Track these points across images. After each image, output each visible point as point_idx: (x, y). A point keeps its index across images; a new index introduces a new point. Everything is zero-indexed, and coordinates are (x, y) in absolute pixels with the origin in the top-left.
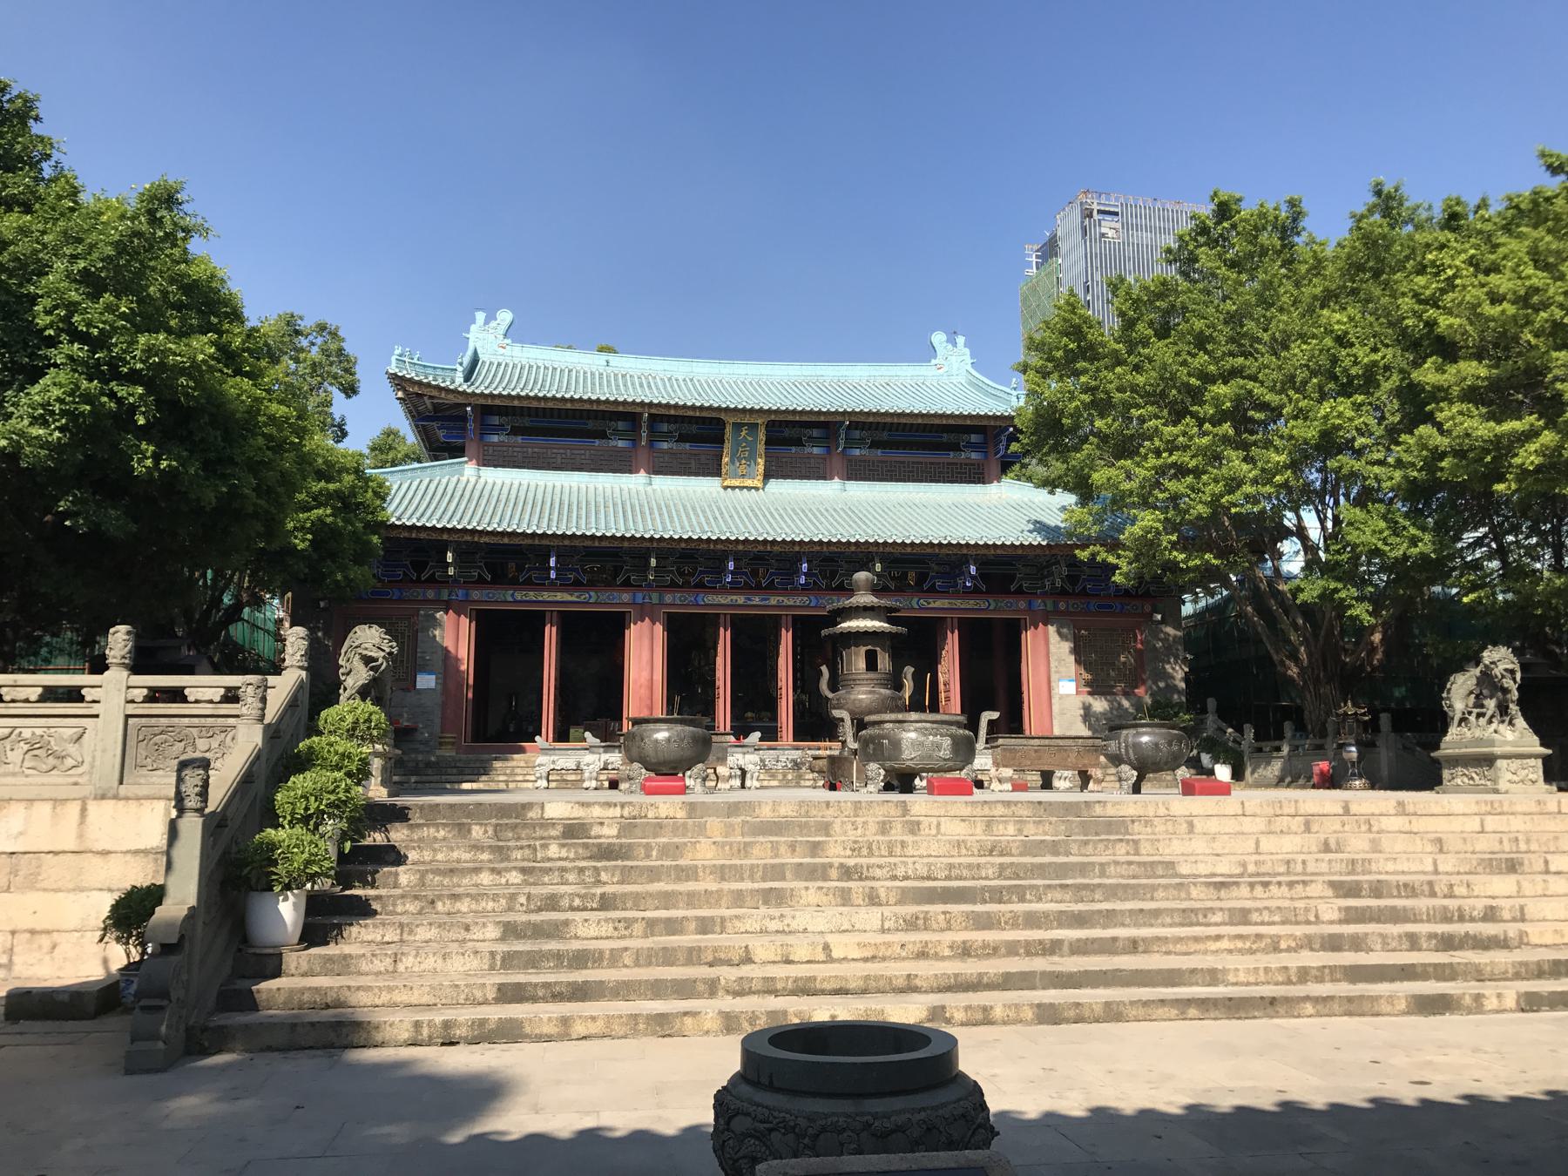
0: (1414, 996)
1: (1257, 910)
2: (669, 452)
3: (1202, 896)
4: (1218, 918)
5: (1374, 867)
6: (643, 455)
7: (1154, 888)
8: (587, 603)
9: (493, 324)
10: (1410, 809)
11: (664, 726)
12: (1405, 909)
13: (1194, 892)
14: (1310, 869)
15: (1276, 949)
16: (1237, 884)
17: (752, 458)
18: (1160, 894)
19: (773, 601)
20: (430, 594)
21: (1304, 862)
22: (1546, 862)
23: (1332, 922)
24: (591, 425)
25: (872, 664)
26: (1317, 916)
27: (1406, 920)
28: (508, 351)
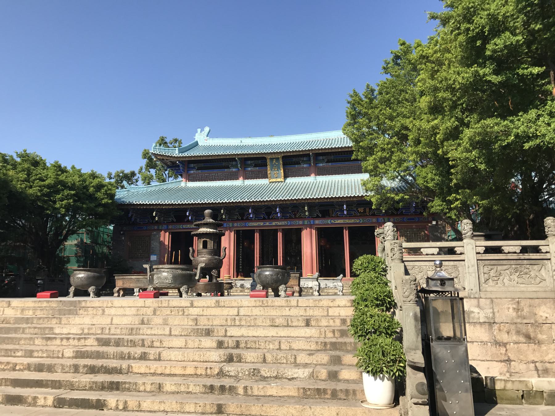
0: (6, 395)
1: (37, 351)
2: (251, 171)
3: (40, 343)
4: (19, 354)
5: (141, 332)
6: (241, 172)
7: (20, 339)
8: (287, 225)
9: (203, 132)
10: (222, 304)
11: (83, 272)
12: (103, 352)
13: (37, 342)
14: (112, 331)
15: (14, 370)
16: (55, 338)
17: (279, 169)
18: (22, 342)
19: (274, 224)
20: (156, 227)
21: (110, 329)
22: (226, 331)
23: (69, 358)
24: (224, 164)
25: (205, 246)
26: (63, 355)
27: (103, 358)
28: (208, 141)
